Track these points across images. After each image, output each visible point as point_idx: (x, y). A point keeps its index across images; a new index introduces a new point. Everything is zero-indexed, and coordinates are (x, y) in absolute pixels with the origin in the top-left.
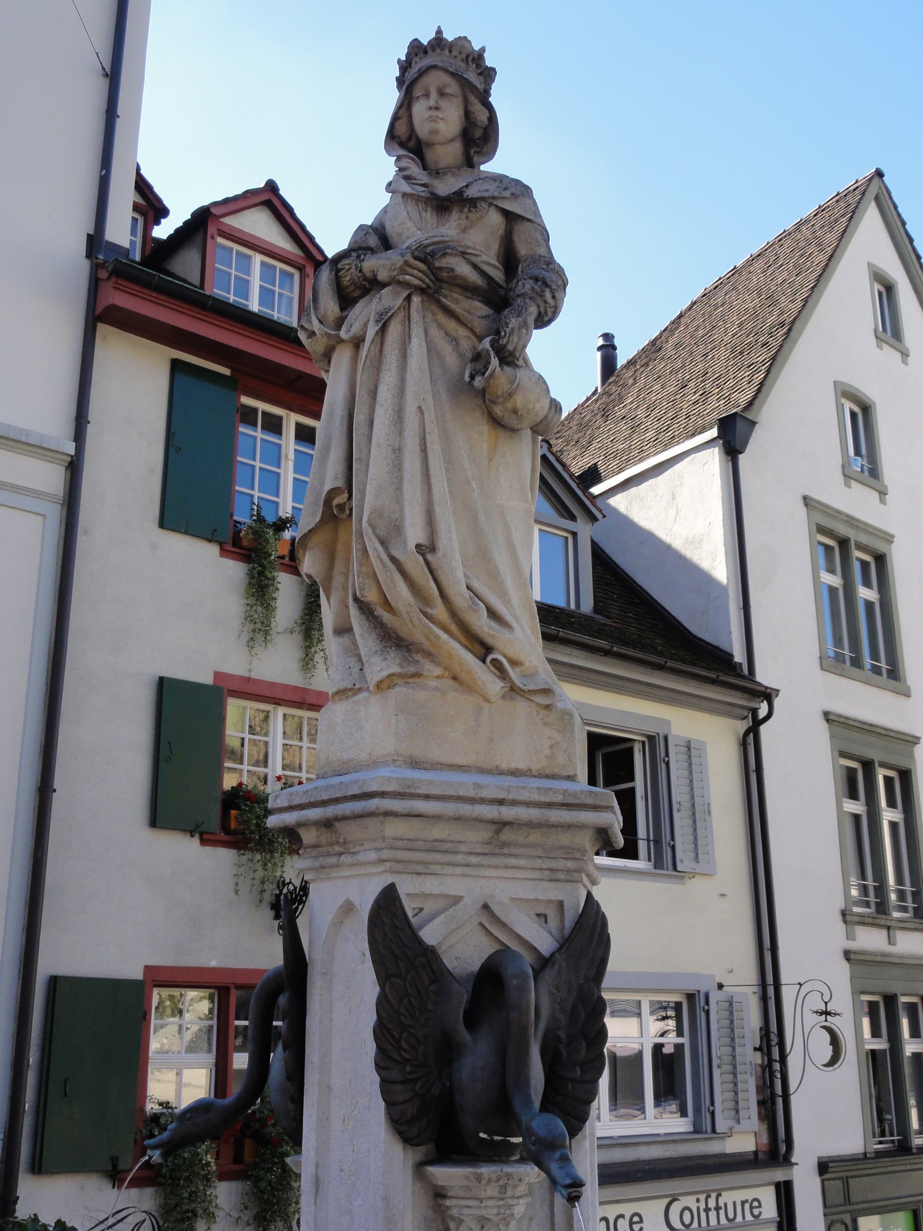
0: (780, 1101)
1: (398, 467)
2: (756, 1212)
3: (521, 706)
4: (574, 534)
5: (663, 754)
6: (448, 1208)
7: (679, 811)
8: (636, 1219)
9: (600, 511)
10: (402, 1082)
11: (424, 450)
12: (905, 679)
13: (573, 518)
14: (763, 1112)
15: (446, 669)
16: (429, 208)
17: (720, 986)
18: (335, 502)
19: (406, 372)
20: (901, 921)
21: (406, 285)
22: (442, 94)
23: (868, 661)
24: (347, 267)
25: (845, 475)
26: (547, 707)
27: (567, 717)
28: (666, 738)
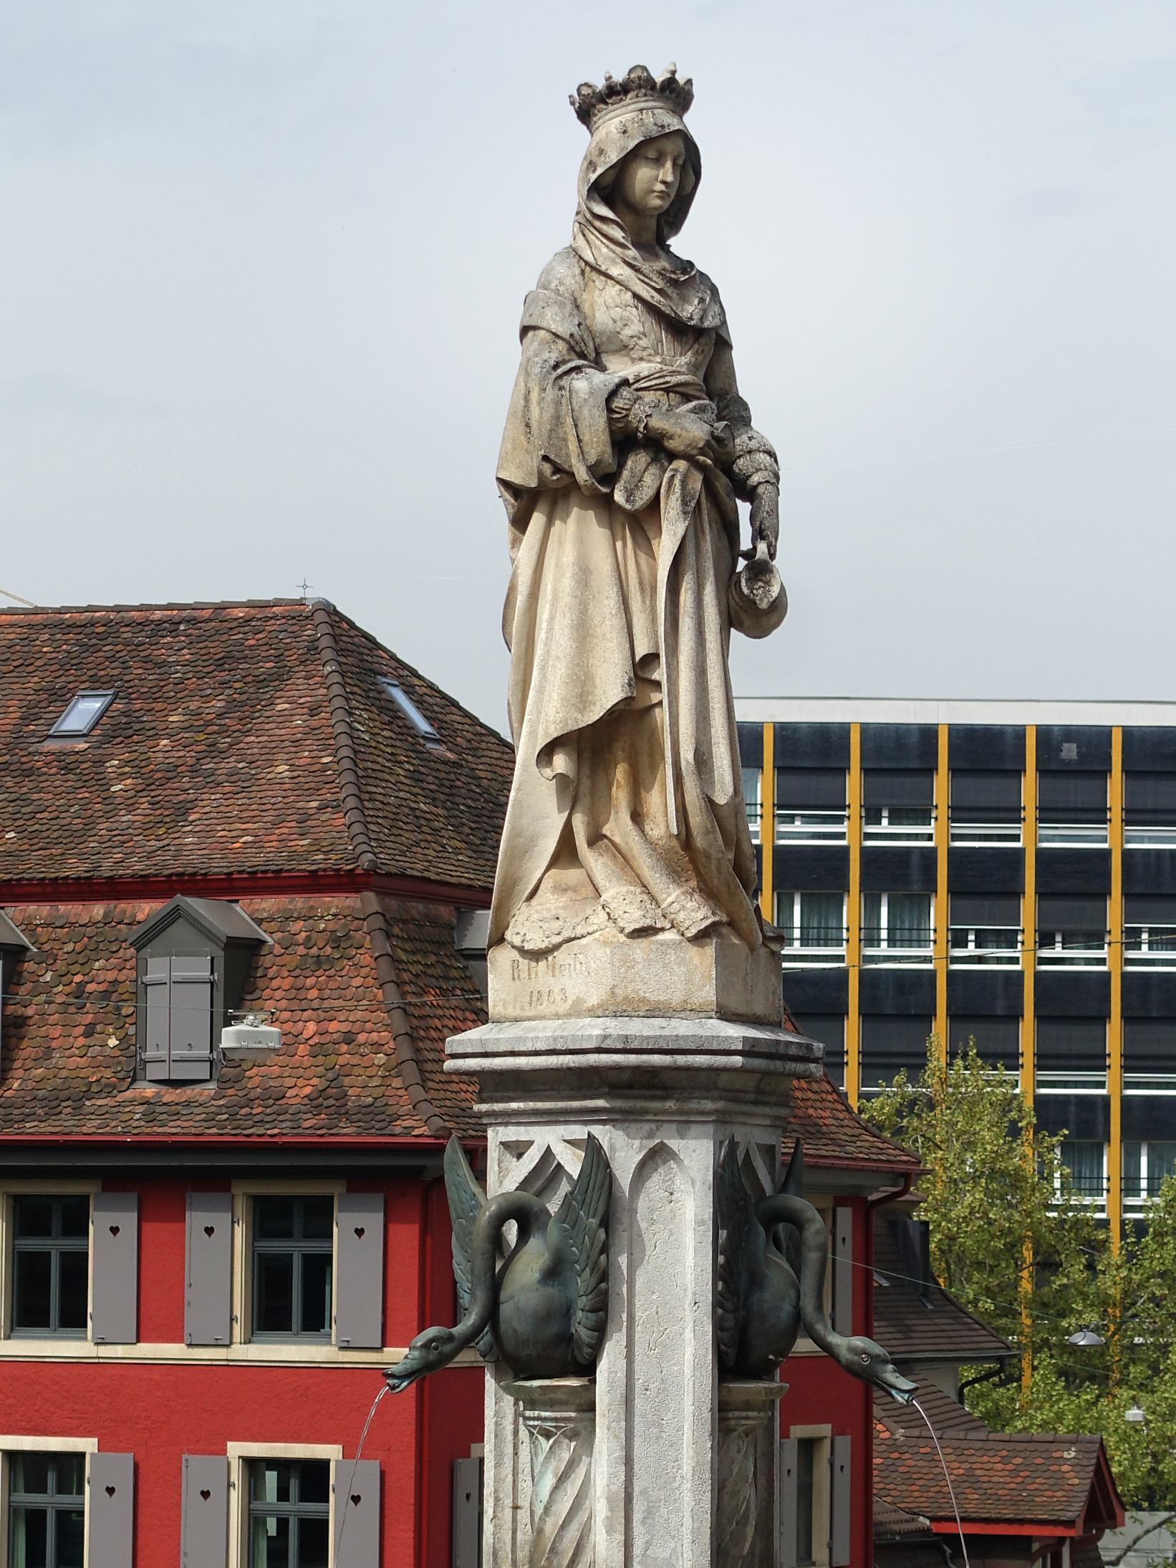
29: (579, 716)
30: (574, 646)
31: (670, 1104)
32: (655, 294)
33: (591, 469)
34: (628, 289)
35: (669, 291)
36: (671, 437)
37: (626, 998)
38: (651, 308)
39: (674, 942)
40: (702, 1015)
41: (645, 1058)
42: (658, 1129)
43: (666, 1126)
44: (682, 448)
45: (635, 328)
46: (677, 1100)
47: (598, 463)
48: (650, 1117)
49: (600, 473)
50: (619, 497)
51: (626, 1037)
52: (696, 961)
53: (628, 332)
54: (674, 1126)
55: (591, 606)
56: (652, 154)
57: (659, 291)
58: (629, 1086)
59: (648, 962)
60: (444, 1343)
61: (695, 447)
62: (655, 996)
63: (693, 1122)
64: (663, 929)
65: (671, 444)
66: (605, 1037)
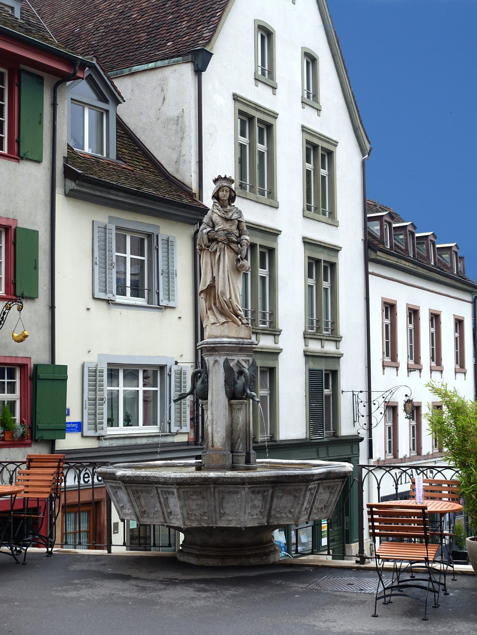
0: (200, 417)
1: (224, 282)
2: (86, 480)
4: (107, 111)
5: (155, 245)
7: (162, 274)
8: (86, 476)
9: (122, 98)
12: (277, 198)
13: (106, 101)
14: (192, 423)
17: (176, 363)
20: (263, 330)
21: (225, 244)
22: (226, 191)
23: (257, 187)
25: (255, 79)
28: (157, 236)
33: (205, 245)
38: (221, 217)
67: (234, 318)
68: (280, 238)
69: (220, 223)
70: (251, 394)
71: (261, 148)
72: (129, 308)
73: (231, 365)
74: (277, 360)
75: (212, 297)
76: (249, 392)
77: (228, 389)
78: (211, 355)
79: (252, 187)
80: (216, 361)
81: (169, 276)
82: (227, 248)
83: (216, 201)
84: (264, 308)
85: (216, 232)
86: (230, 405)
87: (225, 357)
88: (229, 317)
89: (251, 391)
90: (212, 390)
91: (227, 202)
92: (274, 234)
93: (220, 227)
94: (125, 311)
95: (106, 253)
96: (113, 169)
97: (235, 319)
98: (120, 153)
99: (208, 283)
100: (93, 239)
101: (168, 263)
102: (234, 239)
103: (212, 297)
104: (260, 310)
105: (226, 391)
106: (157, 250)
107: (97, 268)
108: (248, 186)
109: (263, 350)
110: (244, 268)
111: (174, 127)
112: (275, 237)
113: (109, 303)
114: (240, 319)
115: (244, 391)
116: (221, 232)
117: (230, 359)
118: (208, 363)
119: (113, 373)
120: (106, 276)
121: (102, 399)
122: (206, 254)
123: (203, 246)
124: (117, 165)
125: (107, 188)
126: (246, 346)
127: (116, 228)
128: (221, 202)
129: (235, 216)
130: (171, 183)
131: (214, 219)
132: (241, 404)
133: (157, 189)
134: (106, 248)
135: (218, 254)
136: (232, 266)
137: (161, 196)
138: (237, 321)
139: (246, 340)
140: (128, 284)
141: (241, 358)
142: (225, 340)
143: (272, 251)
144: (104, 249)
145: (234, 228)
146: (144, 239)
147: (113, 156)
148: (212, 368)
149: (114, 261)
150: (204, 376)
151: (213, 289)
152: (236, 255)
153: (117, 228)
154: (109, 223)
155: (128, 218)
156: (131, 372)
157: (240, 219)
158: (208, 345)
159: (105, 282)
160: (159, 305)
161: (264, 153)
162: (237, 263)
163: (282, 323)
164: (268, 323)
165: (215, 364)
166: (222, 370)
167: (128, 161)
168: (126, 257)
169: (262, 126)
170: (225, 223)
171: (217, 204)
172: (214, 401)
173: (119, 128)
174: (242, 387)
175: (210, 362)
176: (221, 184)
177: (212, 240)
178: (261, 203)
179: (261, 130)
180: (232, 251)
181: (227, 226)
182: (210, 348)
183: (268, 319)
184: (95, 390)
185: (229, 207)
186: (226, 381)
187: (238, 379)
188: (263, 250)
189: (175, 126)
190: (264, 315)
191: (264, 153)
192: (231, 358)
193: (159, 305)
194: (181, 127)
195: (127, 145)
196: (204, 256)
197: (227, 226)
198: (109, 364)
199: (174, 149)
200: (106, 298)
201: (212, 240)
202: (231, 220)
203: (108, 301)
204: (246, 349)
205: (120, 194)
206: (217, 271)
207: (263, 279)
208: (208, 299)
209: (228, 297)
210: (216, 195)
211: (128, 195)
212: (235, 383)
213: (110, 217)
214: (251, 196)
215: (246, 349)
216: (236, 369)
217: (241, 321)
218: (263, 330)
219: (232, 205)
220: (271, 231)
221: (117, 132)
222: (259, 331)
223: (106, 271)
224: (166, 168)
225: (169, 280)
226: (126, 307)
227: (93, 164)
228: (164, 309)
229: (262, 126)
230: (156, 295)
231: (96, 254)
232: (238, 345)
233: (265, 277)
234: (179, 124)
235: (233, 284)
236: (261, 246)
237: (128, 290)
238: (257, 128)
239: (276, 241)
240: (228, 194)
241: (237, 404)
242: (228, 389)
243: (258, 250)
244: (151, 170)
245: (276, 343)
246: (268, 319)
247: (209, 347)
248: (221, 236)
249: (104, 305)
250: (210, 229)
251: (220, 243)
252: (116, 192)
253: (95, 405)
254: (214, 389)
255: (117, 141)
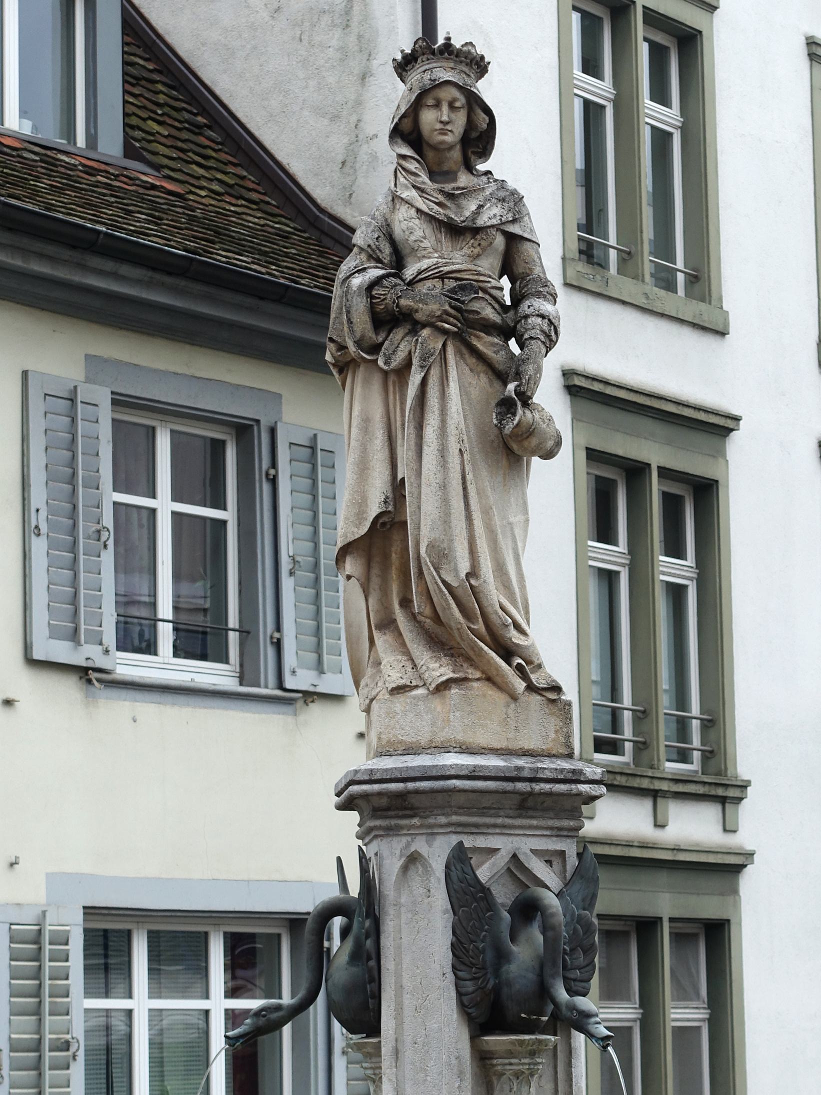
1: (445, 501)
3: (535, 698)
6: (494, 1066)
7: (291, 573)
10: (470, 980)
11: (465, 489)
12: (720, 299)
15: (483, 672)
16: (443, 230)
18: (381, 521)
19: (446, 414)
20: (677, 781)
21: (445, 332)
22: (451, 106)
23: (648, 261)
24: (382, 297)
26: (553, 701)
27: (567, 707)
28: (273, 432)
29: (356, 530)
30: (355, 477)
31: (415, 821)
32: (436, 207)
33: (358, 343)
34: (413, 206)
35: (448, 204)
36: (417, 311)
37: (389, 741)
38: (430, 218)
39: (422, 696)
40: (442, 750)
41: (385, 786)
42: (413, 841)
43: (418, 838)
44: (424, 318)
45: (419, 233)
46: (421, 817)
47: (362, 337)
48: (405, 832)
49: (365, 345)
50: (381, 363)
51: (371, 770)
52: (439, 709)
53: (413, 238)
54: (424, 838)
55: (368, 447)
56: (430, 102)
57: (439, 204)
58: (388, 809)
59: (405, 713)
60: (271, 1012)
61: (434, 316)
62: (409, 737)
63: (489, 834)
64: (416, 687)
65: (419, 316)
66: (356, 772)
67: (490, 661)
68: (736, 444)
69: (426, 244)
70: (573, 1008)
71: (667, 116)
72: (169, 698)
73: (484, 873)
74: (735, 891)
75: (394, 574)
76: (562, 995)
77: (470, 986)
78: (391, 831)
79: (627, 258)
80: (413, 859)
81: (317, 580)
82: (458, 353)
83: (407, 151)
84: (682, 701)
85: (411, 283)
86: (483, 1059)
87: (454, 839)
88: (469, 659)
89: (571, 992)
90: (400, 988)
91: (456, 154)
92: (715, 427)
93: (424, 264)
94: (149, 710)
95: (74, 491)
96: (108, 186)
97: (498, 668)
98: (138, 134)
99: (374, 510)
100: (25, 439)
101: (316, 532)
102: (489, 313)
103: (394, 574)
104: (665, 703)
105: (460, 994)
106: (273, 481)
107: (39, 546)
108: (613, 254)
109: (682, 857)
110: (534, 441)
111: (335, 38)
112: (714, 440)
113: (89, 681)
114: (519, 668)
115: (543, 992)
116: (429, 283)
117: (475, 850)
118: (380, 866)
119: (107, 944)
120: (76, 576)
121: (66, 1046)
122: (367, 382)
123: (352, 348)
124: (122, 174)
125: (74, 247)
126: (547, 787)
127: (114, 402)
128: (430, 154)
129: (492, 214)
130: (327, 242)
131: (398, 231)
132: (532, 1054)
133: (267, 257)
134: (74, 474)
135: (415, 378)
136: (482, 432)
137: (282, 281)
138: (503, 676)
139: (546, 764)
140: (165, 609)
141: (527, 843)
142: (453, 760)
143: (706, 492)
144: (68, 478)
145: (489, 264)
146: (223, 443)
147: (111, 145)
148: (398, 890)
149: (108, 520)
150: (362, 924)
151: (396, 536)
152: (497, 385)
153: (119, 402)
154: (88, 380)
155: (161, 364)
156: (178, 944)
157: (515, 229)
158: (376, 787)
159: (74, 600)
160: (281, 687)
161: (670, 135)
162: (501, 417)
163: (748, 758)
164: (696, 755)
165: (411, 873)
166: (440, 899)
167: (166, 161)
168: (153, 511)
169: (660, 38)
170: (446, 244)
171: (412, 166)
172: (408, 1039)
173: (133, 49)
174: (532, 976)
175: (387, 862)
176: (427, 76)
177: (387, 319)
178: (662, 315)
179: (658, 54)
180: (481, 367)
181: (458, 258)
182: (384, 801)
183: (696, 741)
184: (37, 1012)
185: (464, 179)
186: (457, 948)
187: (513, 939)
188: (675, 489)
189: (338, 33)
190: (682, 726)
191: (670, 135)
192: (481, 842)
193: (281, 687)
194: (360, 37)
195: (167, 109)
196: (358, 390)
197: (458, 258)
198: (90, 911)
199: (335, 118)
200: (78, 660)
201: (387, 319)
202: (476, 231)
203: (84, 673)
204: (549, 802)
205: (125, 269)
206: (412, 454)
207: (676, 593)
208: (375, 582)
209: (464, 567)
210: (407, 125)
211: (158, 276)
212: (502, 956)
213: (172, 431)
214: (626, 288)
215: (549, 802)
216: (504, 895)
217: (524, 676)
218: (677, 781)
219: (481, 167)
220: (702, 416)
221: (125, 63)
222: (664, 786)
223: (75, 560)
224: (308, 188)
225: (318, 595)
226: (156, 696)
227: (32, 167)
228: (300, 703)
229: (660, 38)
230: (271, 652)
231: (39, 496)
232: (509, 786)
233: (684, 588)
234: (354, 23)
235: (486, 512)
236: (665, 473)
237: (166, 635)
238: (644, 49)
239: (720, 453)
240: (460, 121)
241: (511, 1054)
242: (470, 986)
243: (656, 487)
244: (254, 196)
245: (728, 829)
246: (696, 741)
247: (380, 794)
248: (430, 301)
249: (69, 686)
250: (381, 272)
251: (426, 332)
252: (109, 265)
253: (37, 1066)
254: (406, 982)
255: (125, 91)
